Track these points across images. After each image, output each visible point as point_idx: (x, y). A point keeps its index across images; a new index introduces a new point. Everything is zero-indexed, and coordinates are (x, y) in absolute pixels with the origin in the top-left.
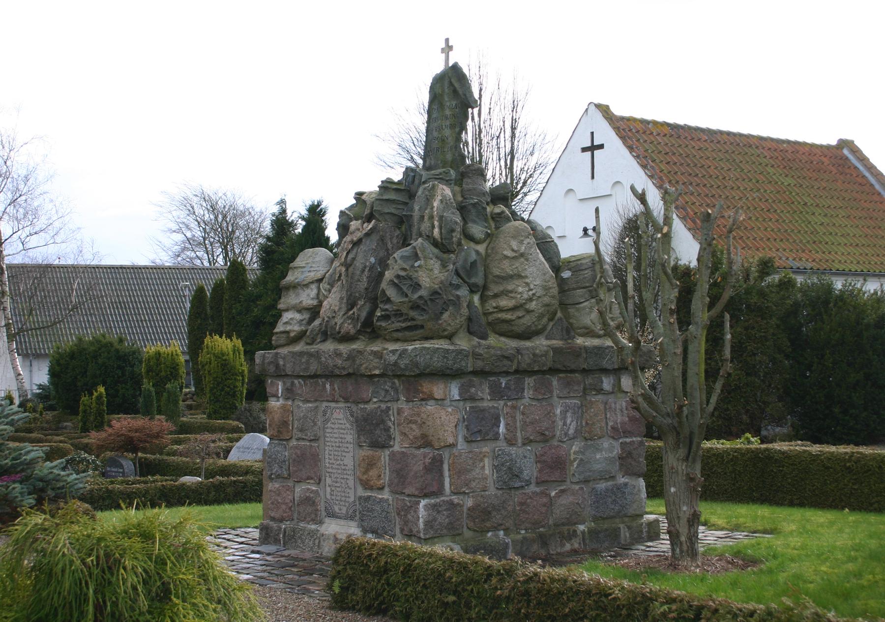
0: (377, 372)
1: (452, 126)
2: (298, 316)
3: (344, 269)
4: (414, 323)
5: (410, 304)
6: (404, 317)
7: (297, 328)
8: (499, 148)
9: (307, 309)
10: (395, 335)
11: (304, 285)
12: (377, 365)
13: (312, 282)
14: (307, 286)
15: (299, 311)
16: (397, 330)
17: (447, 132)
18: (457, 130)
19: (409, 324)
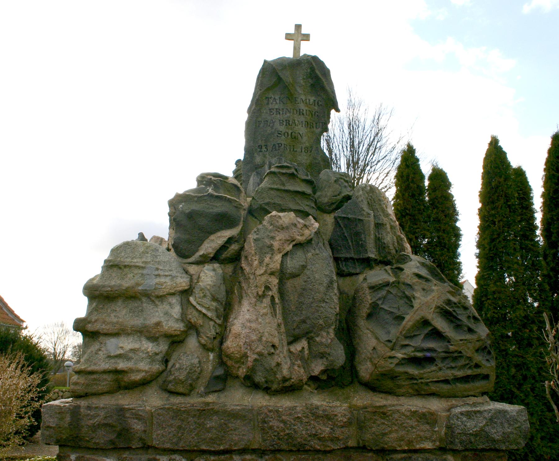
0: (428, 445)
1: (308, 125)
2: (149, 347)
3: (274, 281)
4: (478, 371)
5: (478, 344)
6: (462, 362)
7: (144, 366)
8: (394, 164)
9: (167, 336)
10: (434, 388)
11: (158, 297)
12: (428, 434)
13: (173, 294)
14: (161, 298)
15: (153, 339)
16: (446, 381)
17: (302, 130)
18: (318, 131)
19: (469, 372)
